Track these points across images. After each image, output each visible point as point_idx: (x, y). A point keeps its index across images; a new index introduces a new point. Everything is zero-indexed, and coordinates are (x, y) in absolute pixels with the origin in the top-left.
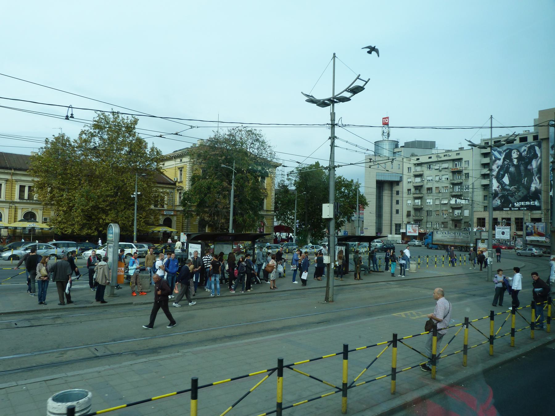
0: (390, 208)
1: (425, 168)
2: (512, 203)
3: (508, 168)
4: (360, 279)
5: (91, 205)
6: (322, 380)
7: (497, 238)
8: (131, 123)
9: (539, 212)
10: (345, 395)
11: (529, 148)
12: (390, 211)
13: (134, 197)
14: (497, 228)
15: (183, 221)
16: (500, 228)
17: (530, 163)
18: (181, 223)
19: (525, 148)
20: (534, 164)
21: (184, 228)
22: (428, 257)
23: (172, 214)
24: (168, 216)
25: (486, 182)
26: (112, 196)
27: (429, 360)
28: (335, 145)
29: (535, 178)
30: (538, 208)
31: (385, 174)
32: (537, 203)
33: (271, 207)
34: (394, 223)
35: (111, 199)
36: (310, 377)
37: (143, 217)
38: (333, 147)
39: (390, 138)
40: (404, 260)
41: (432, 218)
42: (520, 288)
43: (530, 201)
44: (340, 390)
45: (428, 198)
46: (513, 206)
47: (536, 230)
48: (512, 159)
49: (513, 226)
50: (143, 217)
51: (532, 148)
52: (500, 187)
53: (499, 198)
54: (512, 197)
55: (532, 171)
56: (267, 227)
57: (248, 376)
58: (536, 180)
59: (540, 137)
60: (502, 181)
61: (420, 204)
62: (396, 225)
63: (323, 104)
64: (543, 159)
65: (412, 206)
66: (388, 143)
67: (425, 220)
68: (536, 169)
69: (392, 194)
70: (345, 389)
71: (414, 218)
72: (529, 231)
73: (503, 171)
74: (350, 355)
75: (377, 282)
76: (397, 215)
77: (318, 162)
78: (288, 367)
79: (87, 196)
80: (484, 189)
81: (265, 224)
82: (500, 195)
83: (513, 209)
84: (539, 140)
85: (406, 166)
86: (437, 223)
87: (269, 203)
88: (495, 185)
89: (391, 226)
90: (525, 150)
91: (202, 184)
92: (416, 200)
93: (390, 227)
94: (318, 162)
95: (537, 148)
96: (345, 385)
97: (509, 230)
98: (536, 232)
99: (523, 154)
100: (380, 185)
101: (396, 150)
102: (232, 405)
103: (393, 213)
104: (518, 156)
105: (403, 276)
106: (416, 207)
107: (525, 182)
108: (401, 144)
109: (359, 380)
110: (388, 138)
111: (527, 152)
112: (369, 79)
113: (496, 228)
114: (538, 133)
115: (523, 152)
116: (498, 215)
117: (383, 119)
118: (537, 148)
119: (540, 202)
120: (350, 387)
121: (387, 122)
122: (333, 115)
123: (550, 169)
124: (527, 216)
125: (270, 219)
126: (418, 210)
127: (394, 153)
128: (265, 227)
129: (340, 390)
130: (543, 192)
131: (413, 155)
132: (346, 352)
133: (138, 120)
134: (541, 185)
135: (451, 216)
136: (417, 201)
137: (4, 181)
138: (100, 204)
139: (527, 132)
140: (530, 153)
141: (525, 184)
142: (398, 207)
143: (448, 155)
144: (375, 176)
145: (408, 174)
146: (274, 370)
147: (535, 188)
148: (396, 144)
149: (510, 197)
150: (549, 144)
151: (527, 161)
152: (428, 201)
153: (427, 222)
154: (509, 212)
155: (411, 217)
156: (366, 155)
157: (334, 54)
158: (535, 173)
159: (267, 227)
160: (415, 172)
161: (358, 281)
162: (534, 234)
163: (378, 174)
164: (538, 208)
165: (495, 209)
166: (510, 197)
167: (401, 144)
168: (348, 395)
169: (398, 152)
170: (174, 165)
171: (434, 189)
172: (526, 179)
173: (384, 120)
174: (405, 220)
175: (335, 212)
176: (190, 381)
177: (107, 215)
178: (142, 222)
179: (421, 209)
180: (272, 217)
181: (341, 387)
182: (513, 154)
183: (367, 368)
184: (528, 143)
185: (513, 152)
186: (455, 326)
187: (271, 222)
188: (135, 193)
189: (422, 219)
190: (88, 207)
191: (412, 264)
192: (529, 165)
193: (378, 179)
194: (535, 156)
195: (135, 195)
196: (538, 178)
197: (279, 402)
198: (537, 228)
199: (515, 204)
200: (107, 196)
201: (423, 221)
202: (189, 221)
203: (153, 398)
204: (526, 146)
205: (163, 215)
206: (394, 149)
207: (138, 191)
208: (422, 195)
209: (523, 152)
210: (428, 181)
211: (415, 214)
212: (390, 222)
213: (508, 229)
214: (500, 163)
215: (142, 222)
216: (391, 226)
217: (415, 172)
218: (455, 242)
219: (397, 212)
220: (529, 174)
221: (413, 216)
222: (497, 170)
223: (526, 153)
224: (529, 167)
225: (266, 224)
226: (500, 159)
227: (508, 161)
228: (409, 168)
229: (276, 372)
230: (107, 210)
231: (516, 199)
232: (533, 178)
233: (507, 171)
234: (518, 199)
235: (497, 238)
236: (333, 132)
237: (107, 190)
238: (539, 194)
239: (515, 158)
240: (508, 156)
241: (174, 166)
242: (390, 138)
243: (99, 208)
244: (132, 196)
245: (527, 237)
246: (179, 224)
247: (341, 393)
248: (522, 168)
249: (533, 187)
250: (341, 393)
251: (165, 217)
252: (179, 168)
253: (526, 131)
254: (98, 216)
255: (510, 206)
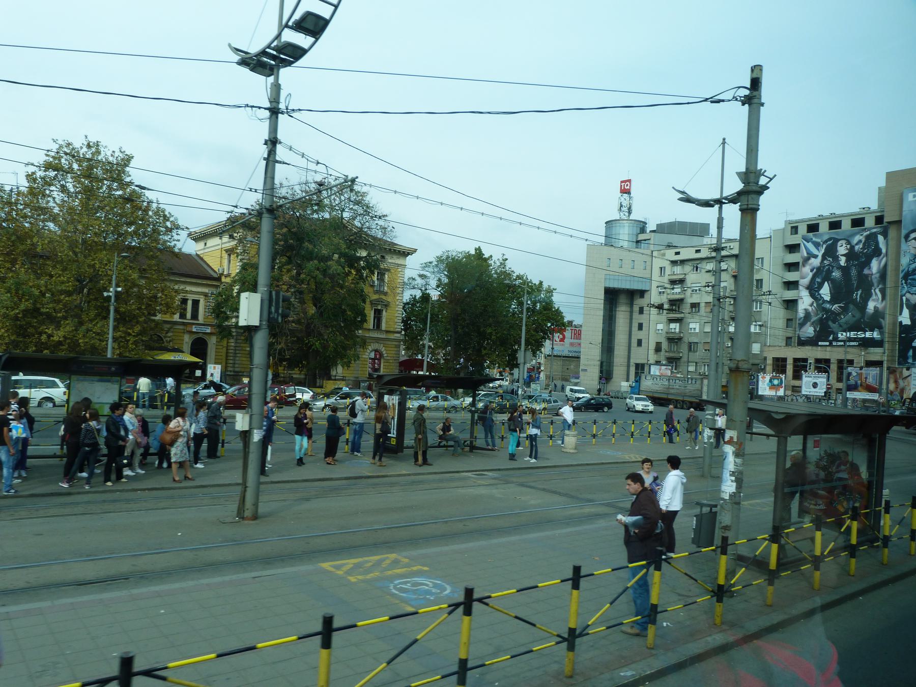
0: (627, 337)
1: (688, 268)
2: (833, 333)
3: (829, 272)
4: (425, 462)
5: (22, 307)
6: (534, 622)
7: (803, 393)
8: (117, 164)
9: (879, 350)
10: (571, 648)
11: (867, 237)
12: (627, 341)
13: (110, 297)
14: (806, 377)
15: (229, 345)
16: (811, 377)
17: (867, 263)
18: (225, 349)
19: (861, 237)
20: (875, 265)
21: (229, 358)
22: (650, 423)
23: (209, 331)
24: (200, 335)
25: (790, 295)
26: (69, 294)
27: (767, 581)
28: (278, 158)
29: (875, 291)
30: (878, 344)
31: (620, 278)
32: (876, 335)
33: (396, 326)
34: (633, 361)
35: (67, 299)
36: (516, 617)
37: (133, 334)
38: (271, 163)
39: (632, 217)
40: (538, 427)
41: (696, 356)
42: (676, 506)
43: (865, 331)
44: (564, 640)
45: (692, 320)
46: (836, 339)
47: (864, 380)
48: (838, 257)
49: (834, 374)
50: (133, 334)
51: (872, 238)
52: (815, 305)
53: (812, 324)
54: (835, 323)
55: (870, 279)
56: (387, 361)
57: (355, 626)
58: (876, 294)
59: (886, 220)
60: (819, 294)
61: (677, 330)
62: (637, 365)
63: (707, 204)
64: (890, 258)
65: (664, 335)
66: (628, 225)
67: (685, 359)
68: (878, 275)
69: (631, 312)
70: (571, 638)
71: (667, 354)
72: (852, 382)
73: (820, 276)
74: (583, 583)
75: (458, 472)
76: (640, 348)
77: (479, 247)
78: (480, 600)
79: (17, 290)
80: (787, 308)
81: (383, 354)
82: (814, 319)
83: (834, 344)
84: (885, 224)
85: (658, 263)
86: (705, 365)
87: (393, 318)
88: (805, 303)
89: (628, 366)
90: (860, 241)
91: (245, 278)
92: (671, 324)
93: (626, 368)
94: (479, 247)
95: (881, 238)
96: (572, 631)
97: (825, 380)
98: (863, 384)
99: (857, 248)
100: (612, 296)
101: (641, 237)
102: (387, 660)
103: (632, 344)
104: (847, 251)
105: (533, 461)
106: (671, 336)
107: (858, 297)
108: (651, 226)
109: (596, 624)
110: (629, 216)
111: (864, 245)
112: (775, 176)
113: (804, 376)
114: (883, 211)
115: (856, 244)
116: (810, 353)
117: (622, 182)
118: (881, 238)
119: (882, 333)
120: (581, 635)
121: (628, 187)
122: (277, 87)
123: (901, 275)
124: (859, 356)
125: (393, 346)
126: (674, 340)
127: (638, 242)
128: (382, 361)
129: (564, 640)
130: (887, 317)
131: (669, 246)
132: (576, 578)
133: (133, 157)
134: (884, 302)
135: (729, 353)
136: (673, 326)
137: (202, 297)
138: (43, 308)
139: (866, 209)
140: (869, 246)
141: (858, 300)
142: (641, 335)
143: (728, 248)
144: (603, 281)
145: (660, 279)
146: (457, 605)
147: (875, 307)
148: (642, 227)
149: (830, 323)
150: (901, 232)
151: (863, 260)
152: (692, 326)
153: (688, 362)
154: (829, 349)
155: (663, 353)
156: (588, 243)
157: (724, 139)
158: (875, 281)
159: (387, 361)
160: (671, 275)
161: (418, 468)
162: (860, 388)
163: (608, 277)
164: (878, 344)
165: (802, 343)
166: (830, 323)
167: (651, 226)
168: (577, 648)
169: (645, 240)
170: (219, 245)
171: (702, 305)
172: (859, 292)
173: (623, 184)
174: (652, 358)
175: (270, 312)
176: (572, 567)
177: (58, 327)
178: (131, 342)
179: (680, 339)
180: (397, 343)
181: (566, 636)
182: (839, 248)
183: (611, 603)
184: (866, 229)
185: (839, 243)
186: (593, 575)
187: (394, 356)
188: (111, 289)
189: (681, 357)
190: (18, 311)
191: (568, 435)
192: (867, 268)
193: (607, 286)
194: (877, 252)
195: (111, 293)
196: (880, 291)
197: (463, 657)
198: (866, 378)
199: (839, 335)
200: (62, 292)
201: (683, 360)
202: (238, 345)
203: (359, 624)
204: (862, 235)
205: (191, 332)
206: (637, 236)
207: (118, 286)
208: (682, 315)
209: (856, 244)
210: (693, 291)
211: (670, 347)
212: (626, 360)
213: (823, 377)
214: (816, 262)
215: (131, 342)
216: (628, 366)
217: (671, 275)
218: (668, 394)
219: (640, 343)
220: (865, 284)
221: (666, 351)
222: (811, 275)
223: (861, 246)
224: (866, 271)
225: (385, 355)
226: (816, 257)
227: (831, 260)
228: (661, 268)
229: (461, 609)
230: (59, 317)
231: (841, 326)
232: (873, 290)
233: (827, 277)
234: (845, 326)
235: (803, 393)
236: (274, 129)
237: (63, 283)
238: (881, 320)
239: (841, 255)
240: (831, 251)
241: (220, 247)
242: (632, 217)
243: (42, 314)
244: (105, 294)
245: (848, 392)
246: (221, 350)
247: (565, 645)
248: (854, 272)
249: (871, 306)
250: (565, 645)
251: (195, 336)
252: (226, 251)
253: (864, 208)
254: (39, 327)
255: (831, 338)
